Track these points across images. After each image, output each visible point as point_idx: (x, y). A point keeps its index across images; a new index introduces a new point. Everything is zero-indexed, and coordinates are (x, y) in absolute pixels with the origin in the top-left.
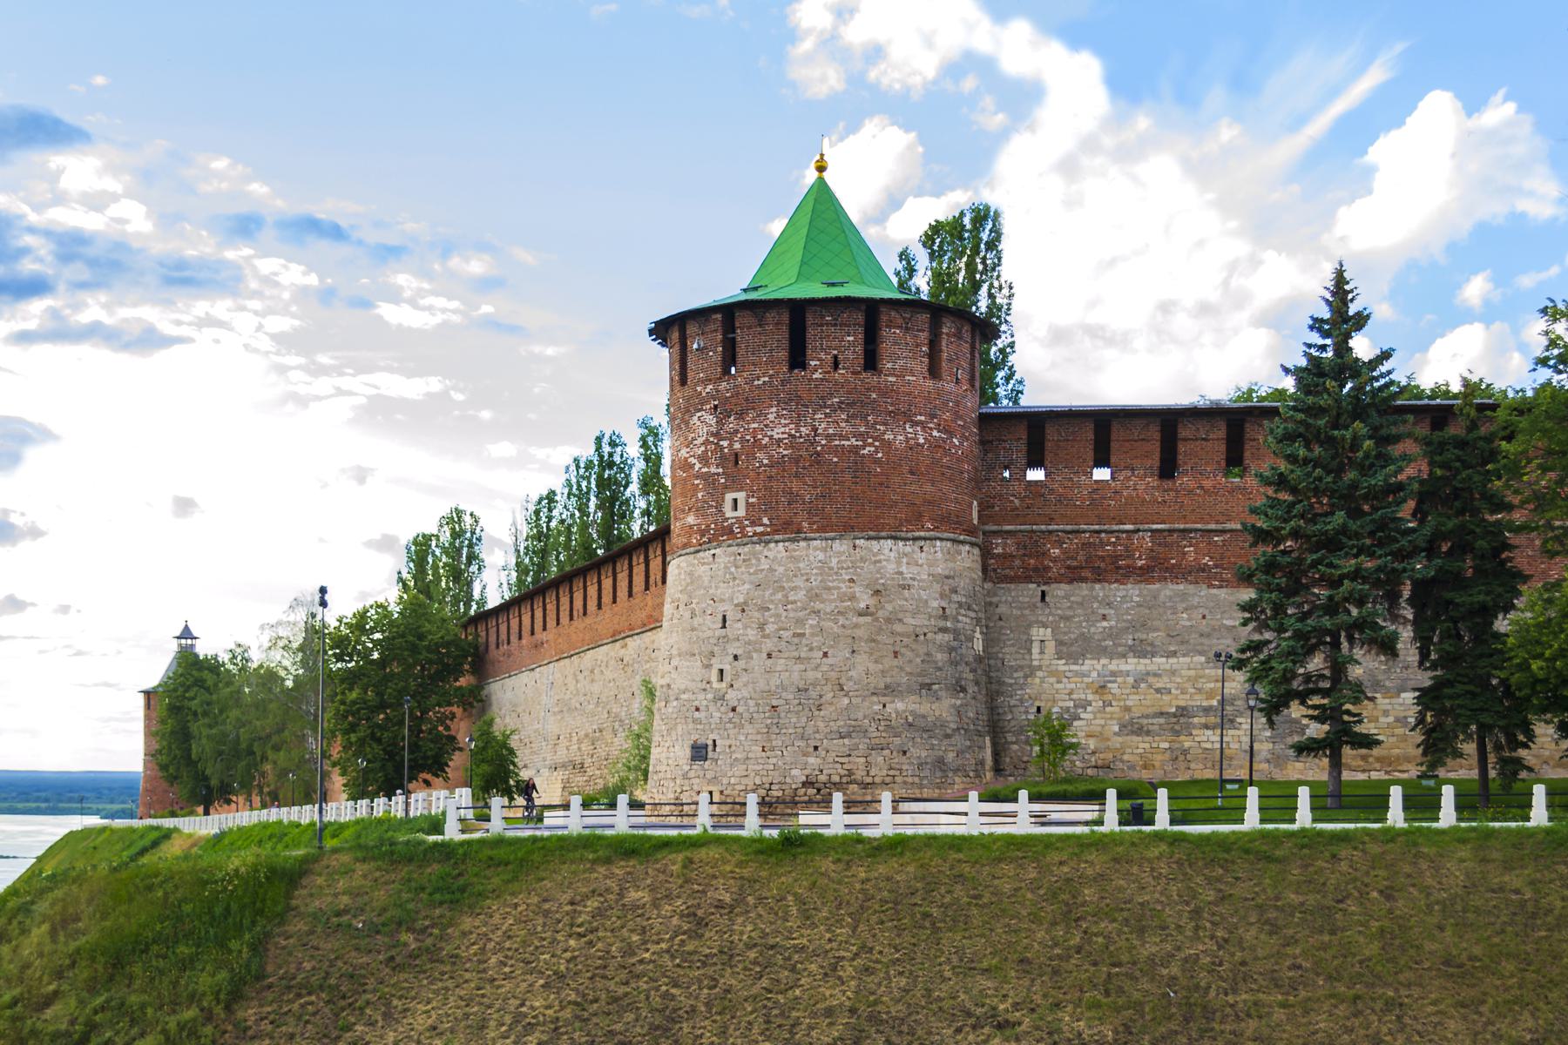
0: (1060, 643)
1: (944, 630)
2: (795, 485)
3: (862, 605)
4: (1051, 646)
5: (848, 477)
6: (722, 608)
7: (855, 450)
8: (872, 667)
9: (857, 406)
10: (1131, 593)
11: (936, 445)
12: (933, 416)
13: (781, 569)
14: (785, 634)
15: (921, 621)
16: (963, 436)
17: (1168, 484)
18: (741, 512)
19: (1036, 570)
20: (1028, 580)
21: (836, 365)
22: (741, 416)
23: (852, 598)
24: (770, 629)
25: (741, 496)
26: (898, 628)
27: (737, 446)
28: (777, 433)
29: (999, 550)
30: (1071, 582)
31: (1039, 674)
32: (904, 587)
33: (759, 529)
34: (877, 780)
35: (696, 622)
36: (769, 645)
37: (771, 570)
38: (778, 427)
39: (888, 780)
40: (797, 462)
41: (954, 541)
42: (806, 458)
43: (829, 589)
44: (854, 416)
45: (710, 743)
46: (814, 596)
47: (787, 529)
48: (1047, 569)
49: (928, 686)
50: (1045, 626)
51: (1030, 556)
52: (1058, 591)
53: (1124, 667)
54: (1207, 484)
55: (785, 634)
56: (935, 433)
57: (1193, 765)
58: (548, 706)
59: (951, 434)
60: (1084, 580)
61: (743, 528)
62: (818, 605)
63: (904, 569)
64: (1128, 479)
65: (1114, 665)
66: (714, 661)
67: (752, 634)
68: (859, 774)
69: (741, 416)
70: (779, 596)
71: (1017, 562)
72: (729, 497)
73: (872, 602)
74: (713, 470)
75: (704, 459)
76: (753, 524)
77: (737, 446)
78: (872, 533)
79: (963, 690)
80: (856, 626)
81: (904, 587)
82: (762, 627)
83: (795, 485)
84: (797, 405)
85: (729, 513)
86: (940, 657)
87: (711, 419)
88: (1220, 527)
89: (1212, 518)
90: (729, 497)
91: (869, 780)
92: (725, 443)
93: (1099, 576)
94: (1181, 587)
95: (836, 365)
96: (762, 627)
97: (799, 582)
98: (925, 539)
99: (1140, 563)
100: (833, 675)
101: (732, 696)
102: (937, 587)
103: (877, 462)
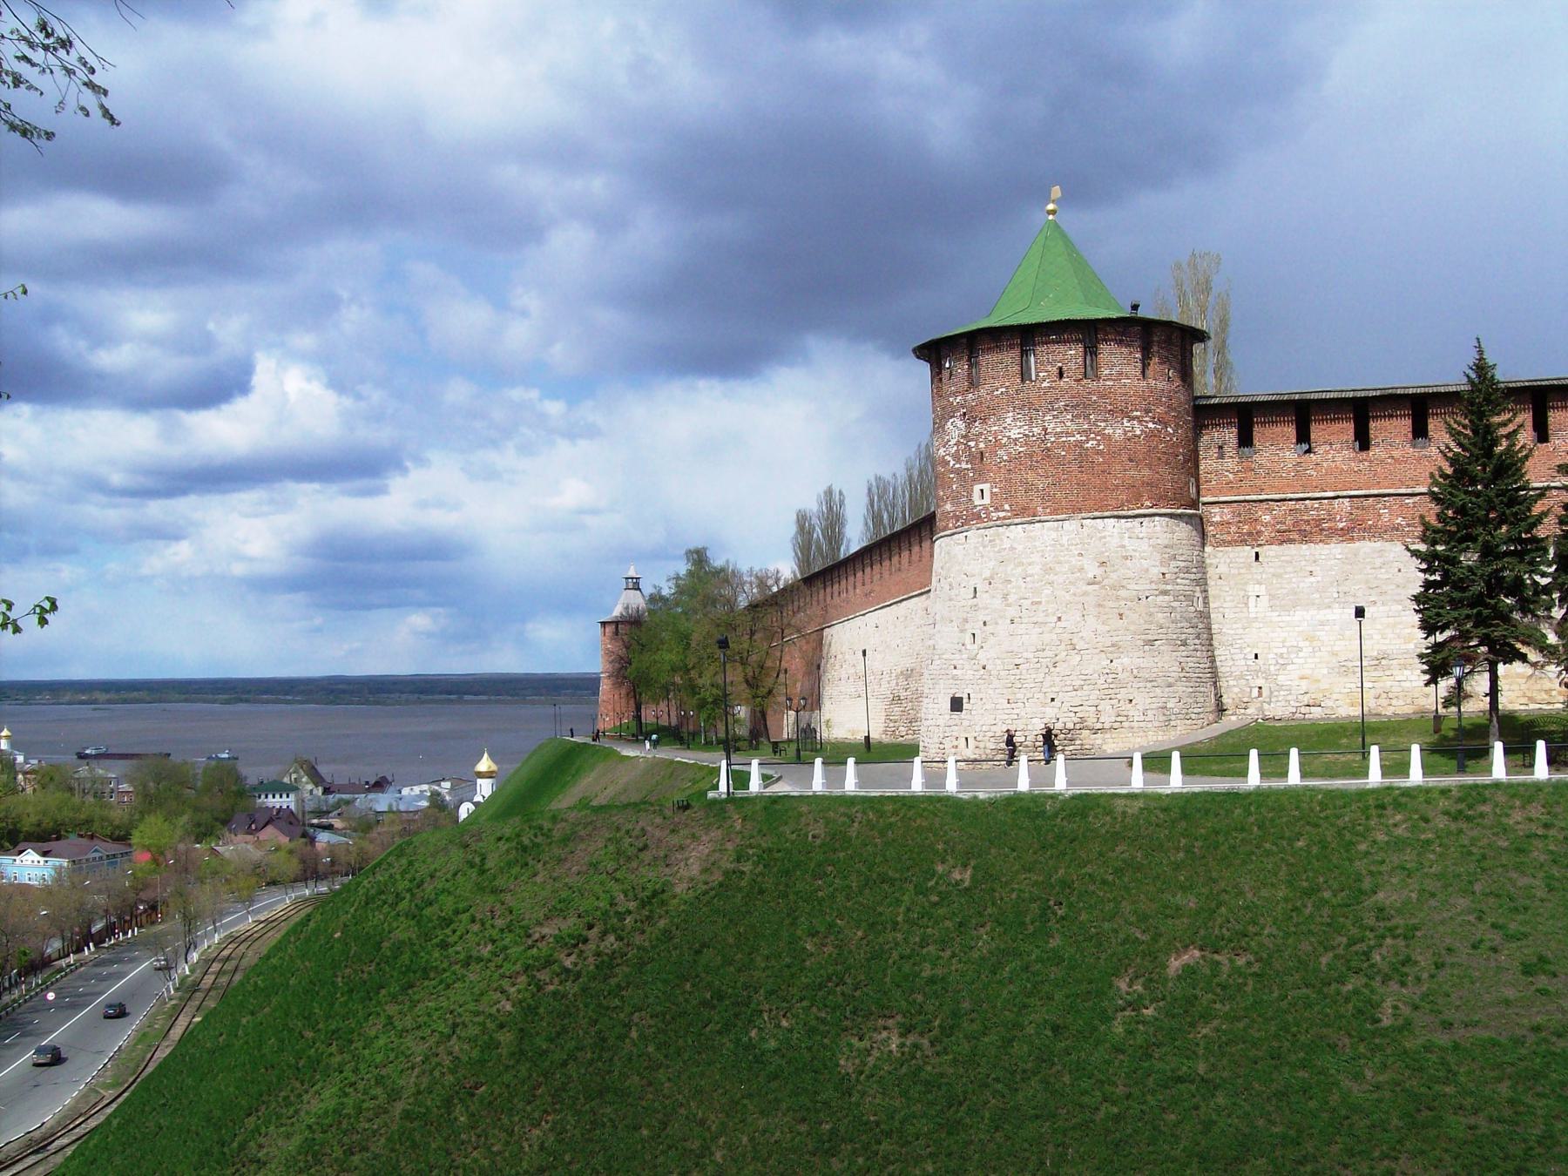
0: (1272, 597)
1: (1165, 593)
2: (1030, 476)
3: (1091, 575)
4: (1264, 600)
5: (1075, 467)
6: (972, 582)
7: (1079, 444)
8: (1101, 628)
9: (1080, 407)
10: (1333, 551)
11: (1151, 435)
12: (1147, 411)
13: (1020, 548)
14: (1026, 603)
15: (1144, 586)
16: (1177, 425)
17: (1364, 454)
18: (987, 500)
19: (1250, 534)
20: (1244, 542)
21: (1061, 375)
22: (984, 421)
23: (1081, 569)
24: (1012, 598)
25: (986, 487)
26: (1123, 593)
27: (982, 445)
28: (1014, 433)
29: (1217, 519)
30: (1282, 543)
31: (1256, 625)
32: (1126, 558)
33: (1002, 514)
34: (1107, 726)
35: (953, 592)
36: (1012, 612)
37: (1012, 548)
38: (1013, 428)
39: (1116, 725)
40: (1031, 456)
41: (1171, 516)
42: (1042, 453)
43: (1060, 563)
44: (1078, 416)
45: (965, 697)
46: (1048, 570)
47: (1025, 513)
48: (1259, 533)
49: (1151, 643)
50: (1260, 583)
51: (1245, 523)
52: (1268, 552)
53: (1331, 617)
54: (1396, 454)
55: (1026, 603)
56: (1151, 425)
57: (1394, 702)
58: (868, 669)
59: (1166, 425)
60: (1292, 541)
61: (988, 514)
62: (1052, 577)
63: (1126, 542)
64: (1327, 452)
65: (1324, 615)
66: (967, 626)
67: (997, 603)
68: (1091, 722)
69: (984, 421)
70: (1020, 569)
71: (1234, 529)
72: (977, 488)
73: (1099, 572)
74: (964, 466)
75: (957, 458)
76: (997, 509)
77: (982, 445)
78: (1097, 514)
79: (1184, 644)
80: (1085, 594)
81: (1126, 558)
82: (1005, 597)
83: (1030, 476)
84: (1029, 409)
85: (977, 500)
86: (1160, 617)
87: (960, 423)
88: (1409, 491)
89: (1402, 483)
90: (977, 488)
91: (1099, 726)
92: (972, 444)
93: (1305, 537)
94: (1379, 544)
95: (1061, 375)
96: (1005, 597)
97: (1036, 558)
98: (1145, 516)
99: (1341, 525)
100: (1066, 636)
101: (982, 657)
102: (1158, 557)
103: (1099, 453)
